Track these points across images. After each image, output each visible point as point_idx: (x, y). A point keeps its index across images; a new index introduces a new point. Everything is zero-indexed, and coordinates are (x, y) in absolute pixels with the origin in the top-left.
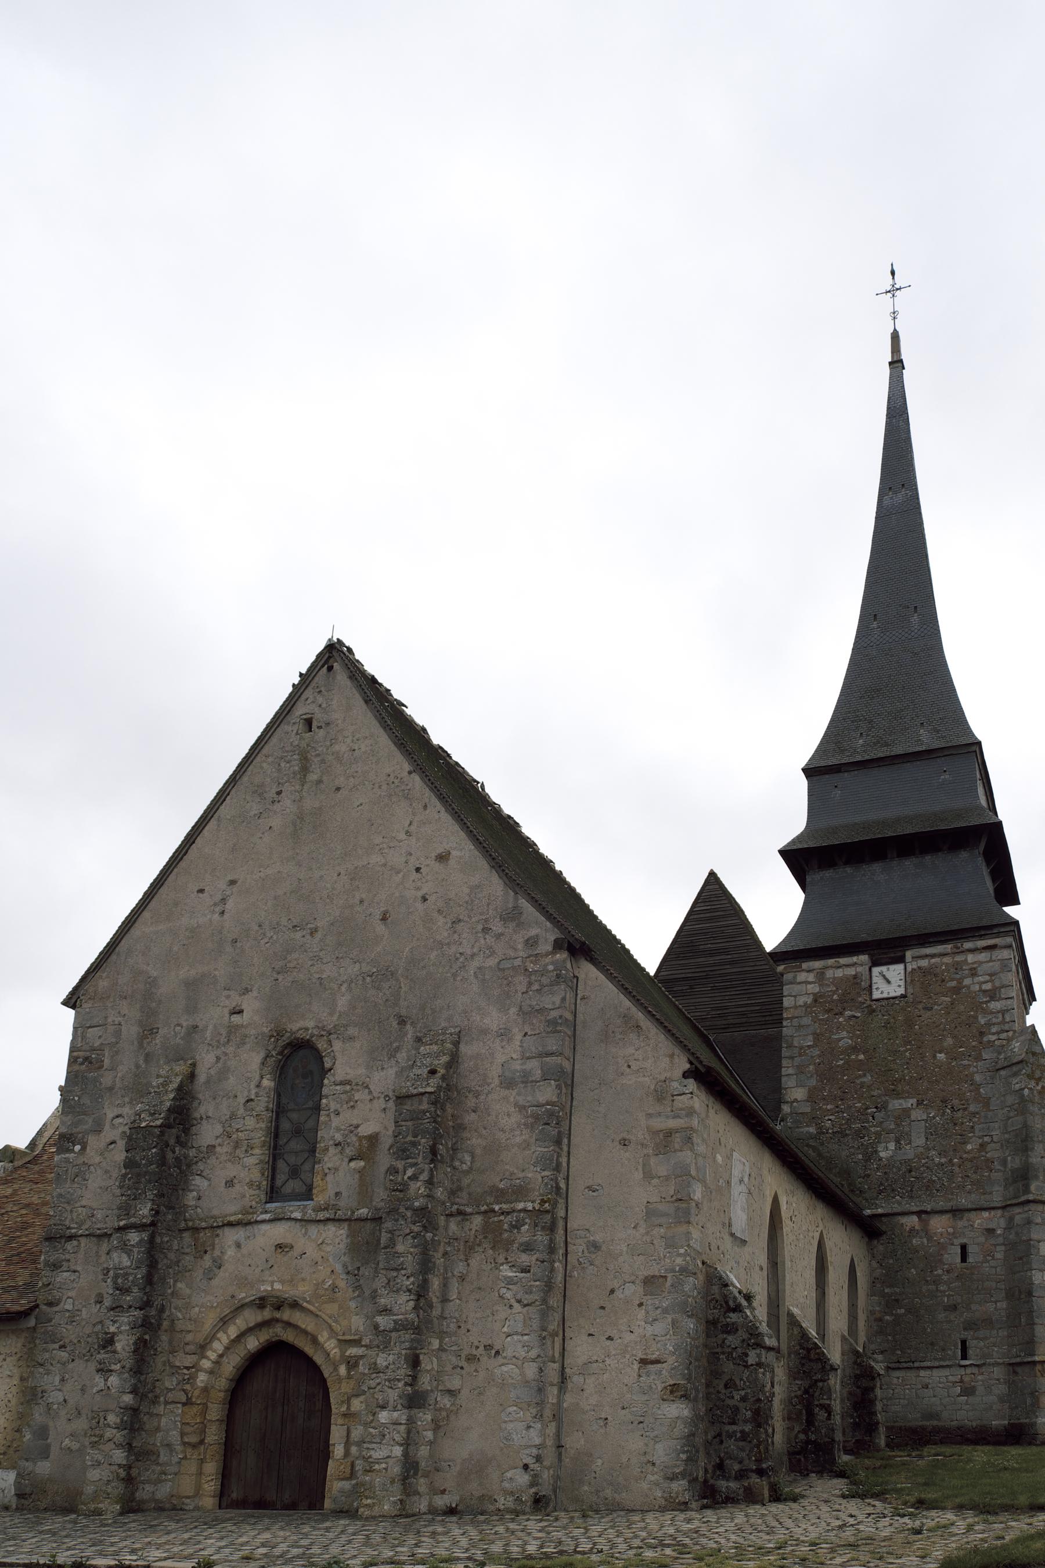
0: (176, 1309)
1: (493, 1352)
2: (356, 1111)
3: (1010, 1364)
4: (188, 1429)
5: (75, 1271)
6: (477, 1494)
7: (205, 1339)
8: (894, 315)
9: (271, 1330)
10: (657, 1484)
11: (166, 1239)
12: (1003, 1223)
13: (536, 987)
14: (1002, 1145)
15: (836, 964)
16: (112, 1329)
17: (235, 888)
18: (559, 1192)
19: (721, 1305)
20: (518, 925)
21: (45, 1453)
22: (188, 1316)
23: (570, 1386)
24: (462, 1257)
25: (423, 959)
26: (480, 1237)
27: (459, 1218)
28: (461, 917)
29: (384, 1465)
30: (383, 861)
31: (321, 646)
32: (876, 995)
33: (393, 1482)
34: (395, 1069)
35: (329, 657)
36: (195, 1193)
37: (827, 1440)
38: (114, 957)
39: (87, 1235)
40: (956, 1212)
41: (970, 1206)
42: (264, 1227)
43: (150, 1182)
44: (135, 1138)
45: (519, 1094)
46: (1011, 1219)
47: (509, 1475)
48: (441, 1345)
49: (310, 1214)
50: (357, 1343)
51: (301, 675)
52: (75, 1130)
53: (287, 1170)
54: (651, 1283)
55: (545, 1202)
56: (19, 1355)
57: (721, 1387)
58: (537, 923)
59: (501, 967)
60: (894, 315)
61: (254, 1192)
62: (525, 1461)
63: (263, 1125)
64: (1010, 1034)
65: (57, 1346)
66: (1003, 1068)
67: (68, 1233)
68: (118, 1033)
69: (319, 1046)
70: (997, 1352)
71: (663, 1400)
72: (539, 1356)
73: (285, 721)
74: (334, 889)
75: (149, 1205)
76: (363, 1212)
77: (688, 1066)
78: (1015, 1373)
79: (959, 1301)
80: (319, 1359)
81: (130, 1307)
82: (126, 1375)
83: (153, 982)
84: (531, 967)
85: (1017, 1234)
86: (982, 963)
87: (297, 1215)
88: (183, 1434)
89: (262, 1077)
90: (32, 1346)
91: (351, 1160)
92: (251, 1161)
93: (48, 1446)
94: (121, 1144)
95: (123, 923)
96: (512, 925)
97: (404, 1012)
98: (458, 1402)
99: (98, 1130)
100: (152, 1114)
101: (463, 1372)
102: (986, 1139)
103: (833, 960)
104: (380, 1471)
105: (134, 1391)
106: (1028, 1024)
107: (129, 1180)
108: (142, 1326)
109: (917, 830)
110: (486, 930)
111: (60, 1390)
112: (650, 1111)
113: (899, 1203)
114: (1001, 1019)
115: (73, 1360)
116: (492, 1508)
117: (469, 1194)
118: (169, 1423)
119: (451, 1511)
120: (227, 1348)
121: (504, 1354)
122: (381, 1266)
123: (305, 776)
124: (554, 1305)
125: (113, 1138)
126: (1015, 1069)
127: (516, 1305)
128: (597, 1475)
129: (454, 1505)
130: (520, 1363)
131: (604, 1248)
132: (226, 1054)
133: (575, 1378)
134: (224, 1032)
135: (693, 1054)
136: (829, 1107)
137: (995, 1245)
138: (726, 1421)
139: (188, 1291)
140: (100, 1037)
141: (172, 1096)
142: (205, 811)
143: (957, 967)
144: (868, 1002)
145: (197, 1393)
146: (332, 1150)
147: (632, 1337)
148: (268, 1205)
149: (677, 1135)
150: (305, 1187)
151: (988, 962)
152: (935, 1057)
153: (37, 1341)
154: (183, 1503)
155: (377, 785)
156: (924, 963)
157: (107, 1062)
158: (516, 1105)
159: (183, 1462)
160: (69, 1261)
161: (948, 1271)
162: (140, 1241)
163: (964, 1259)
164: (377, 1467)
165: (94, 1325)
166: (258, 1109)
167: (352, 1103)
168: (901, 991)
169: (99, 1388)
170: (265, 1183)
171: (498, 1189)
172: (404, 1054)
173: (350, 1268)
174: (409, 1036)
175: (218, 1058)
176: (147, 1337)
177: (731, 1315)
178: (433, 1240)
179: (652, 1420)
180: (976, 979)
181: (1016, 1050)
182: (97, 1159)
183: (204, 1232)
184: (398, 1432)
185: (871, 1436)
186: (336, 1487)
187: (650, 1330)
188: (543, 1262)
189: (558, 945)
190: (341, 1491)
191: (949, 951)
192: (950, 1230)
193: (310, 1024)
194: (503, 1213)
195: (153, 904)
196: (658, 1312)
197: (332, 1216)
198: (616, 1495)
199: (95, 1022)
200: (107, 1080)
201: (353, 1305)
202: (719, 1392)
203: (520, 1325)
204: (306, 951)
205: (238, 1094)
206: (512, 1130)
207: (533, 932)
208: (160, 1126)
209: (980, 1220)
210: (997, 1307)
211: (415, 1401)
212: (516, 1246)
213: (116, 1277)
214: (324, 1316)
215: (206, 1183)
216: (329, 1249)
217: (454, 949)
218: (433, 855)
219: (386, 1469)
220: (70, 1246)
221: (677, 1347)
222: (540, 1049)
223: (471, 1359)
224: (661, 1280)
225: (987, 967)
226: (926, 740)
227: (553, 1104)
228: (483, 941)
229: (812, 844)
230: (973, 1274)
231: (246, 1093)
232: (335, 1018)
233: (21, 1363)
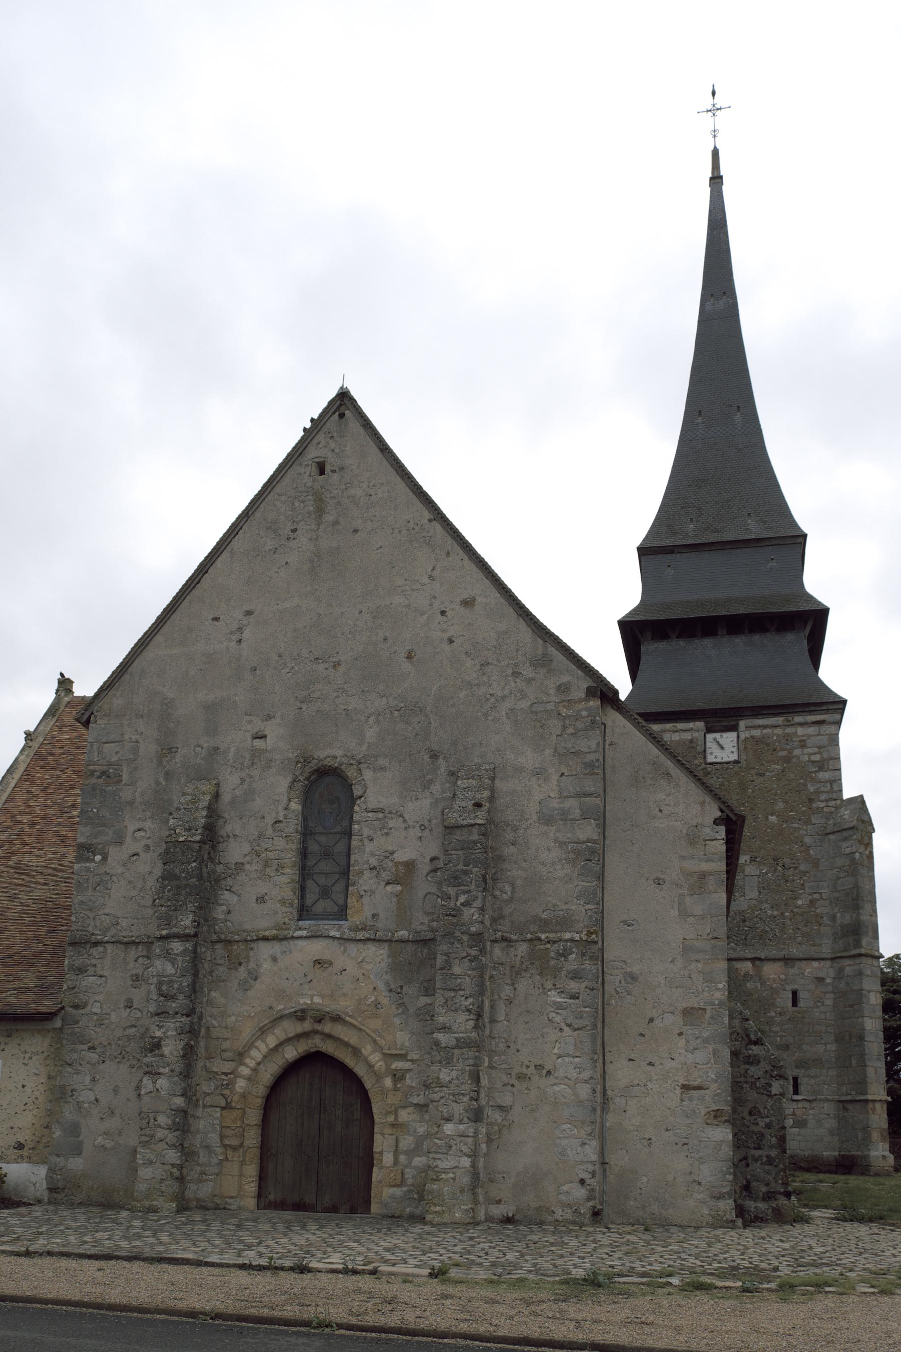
0: (210, 1017)
1: (544, 1072)
3: (840, 1101)
4: (228, 1132)
5: (101, 976)
7: (244, 1047)
8: (715, 134)
9: (309, 1041)
10: (703, 1202)
11: (203, 950)
12: (832, 973)
13: (571, 730)
14: (831, 903)
15: (674, 729)
16: (158, 1034)
18: (599, 923)
19: (742, 1038)
21: (77, 1150)
23: (612, 1106)
24: (509, 981)
25: (452, 698)
26: (527, 963)
27: (504, 944)
29: (451, 1175)
30: (407, 602)
31: (332, 394)
32: (710, 759)
33: (462, 1191)
34: (429, 800)
35: (341, 405)
36: (224, 908)
38: (126, 677)
39: (113, 942)
40: (788, 961)
41: (801, 956)
42: (300, 943)
43: (190, 894)
45: (558, 830)
46: (841, 970)
47: (565, 1188)
48: (490, 1063)
49: (348, 934)
50: (402, 1057)
51: (312, 420)
52: (94, 841)
55: (592, 933)
56: (46, 1054)
57: (746, 1114)
58: (567, 671)
59: (534, 710)
60: (715, 134)
61: (287, 910)
62: (581, 1176)
63: (294, 847)
65: (86, 1047)
66: (833, 833)
68: (135, 750)
69: (349, 774)
71: (707, 1124)
72: (591, 1078)
73: (297, 462)
75: (191, 917)
76: (403, 934)
77: (719, 814)
78: (846, 1109)
80: (360, 1070)
81: (177, 1013)
82: (176, 1079)
84: (564, 712)
85: (847, 984)
88: (222, 1137)
89: (290, 800)
90: (59, 1046)
91: (388, 883)
92: (284, 879)
93: (80, 1143)
95: (136, 645)
96: (542, 671)
97: (435, 747)
98: (510, 1117)
99: (119, 841)
101: (514, 1089)
102: (816, 896)
103: (671, 725)
104: (447, 1180)
106: (846, 795)
107: (169, 891)
108: (190, 1032)
109: (750, 611)
110: (516, 674)
111: (90, 1090)
112: (683, 854)
113: (734, 950)
114: (829, 788)
115: (104, 1062)
116: (550, 1218)
117: (512, 922)
118: (207, 1125)
119: (509, 1220)
120: (265, 1057)
121: (556, 1075)
123: (320, 516)
124: (599, 1033)
125: (136, 851)
126: (845, 834)
127: (566, 1029)
129: (510, 1215)
130: (572, 1083)
132: (251, 777)
133: (617, 1100)
134: (248, 756)
135: (724, 802)
137: (825, 993)
138: (752, 1145)
139: (223, 1000)
140: (117, 753)
141: (204, 813)
142: (218, 543)
145: (236, 1098)
146: (367, 874)
147: (674, 1063)
148: (301, 923)
149: (711, 877)
150: (336, 908)
151: (817, 735)
152: (767, 818)
153: (64, 1042)
154: (226, 1203)
155: (396, 531)
156: (757, 733)
157: (125, 777)
158: (556, 840)
159: (225, 1163)
160: (95, 966)
161: (780, 1014)
163: (795, 1003)
164: (443, 1176)
165: (125, 1029)
166: (287, 830)
167: (386, 831)
168: (734, 757)
169: (148, 1090)
170: (296, 901)
171: (541, 920)
172: (438, 787)
173: (392, 986)
174: (442, 769)
175: (243, 780)
176: (192, 1043)
177: (753, 1047)
181: (846, 817)
182: (120, 870)
183: (238, 946)
184: (466, 1144)
186: (385, 1192)
187: (690, 1058)
188: (592, 990)
190: (393, 1197)
191: (781, 723)
192: (783, 977)
193: (339, 753)
194: (549, 942)
195: (166, 629)
196: (699, 1041)
197: (373, 937)
198: (662, 1211)
200: (126, 794)
201: (397, 1021)
202: (743, 1118)
204: (330, 683)
206: (553, 864)
207: (565, 679)
208: (199, 842)
209: (811, 969)
210: (827, 1049)
212: (564, 973)
213: (160, 984)
214: (367, 1030)
215: (236, 898)
216: (369, 967)
218: (458, 600)
219: (454, 1179)
220: (96, 951)
223: (521, 1077)
224: (701, 1012)
226: (753, 529)
227: (594, 842)
228: (513, 684)
229: (638, 618)
230: (804, 1017)
231: (274, 815)
232: (364, 748)
233: (48, 1062)
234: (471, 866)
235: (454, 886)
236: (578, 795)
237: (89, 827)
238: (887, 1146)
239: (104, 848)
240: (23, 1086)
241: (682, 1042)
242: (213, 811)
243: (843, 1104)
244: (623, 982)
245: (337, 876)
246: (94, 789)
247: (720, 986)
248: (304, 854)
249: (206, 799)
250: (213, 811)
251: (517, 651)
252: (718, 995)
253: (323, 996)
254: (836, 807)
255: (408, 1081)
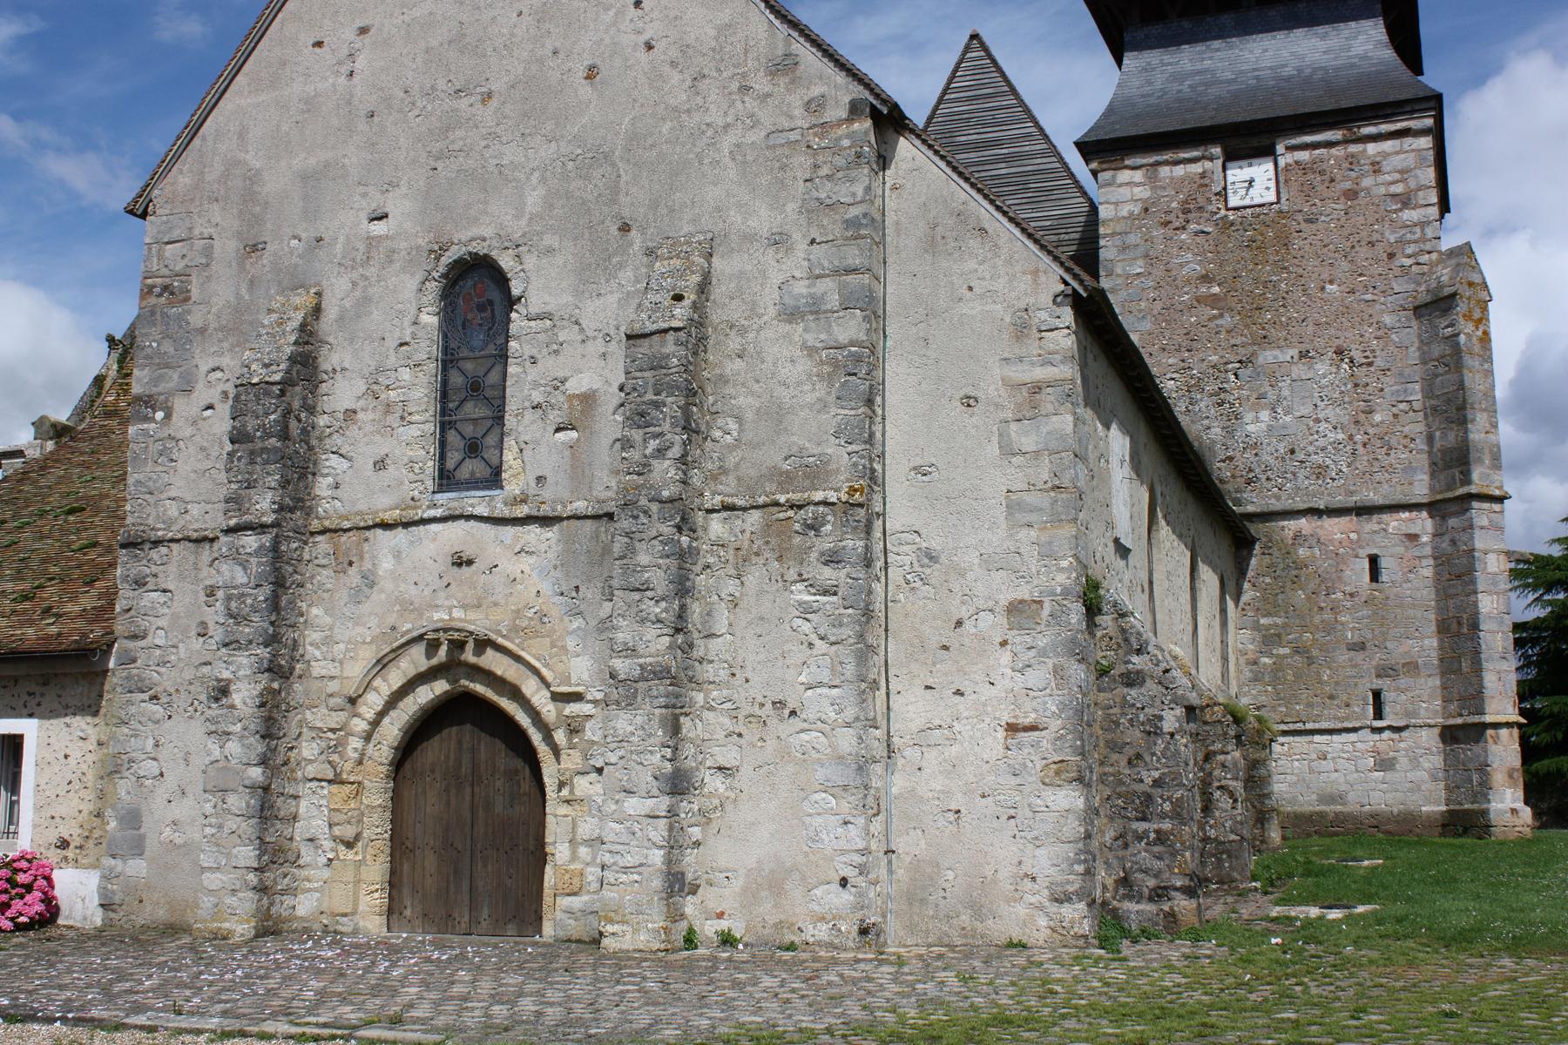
1: (787, 712)
2: (561, 358)
5: (164, 591)
6: (772, 919)
10: (1041, 908)
13: (825, 171)
16: (226, 675)
17: (367, 39)
20: (793, 81)
22: (330, 656)
23: (900, 762)
24: (733, 572)
25: (652, 134)
27: (725, 514)
28: (706, 71)
34: (617, 296)
36: (330, 479)
37: (1233, 837)
41: (1381, 502)
43: (267, 462)
44: (245, 395)
49: (502, 510)
52: (155, 390)
53: (462, 443)
54: (1015, 609)
57: (1123, 763)
58: (821, 78)
62: (842, 874)
64: (1434, 256)
67: (153, 536)
68: (208, 252)
70: (1427, 709)
74: (512, 35)
75: (269, 495)
79: (1369, 636)
81: (250, 642)
83: (253, 177)
84: (815, 142)
85: (1453, 542)
86: (1389, 155)
87: (481, 510)
91: (558, 430)
92: (414, 431)
93: (142, 838)
94: (224, 409)
96: (783, 81)
97: (626, 213)
100: (266, 366)
101: (742, 741)
105: (264, 762)
112: (1006, 355)
117: (739, 479)
118: (313, 812)
122: (615, 583)
127: (818, 643)
128: (948, 894)
131: (943, 559)
133: (908, 752)
134: (362, 247)
136: (1171, 361)
139: (328, 620)
143: (1352, 160)
144: (1223, 212)
145: (348, 766)
146: (529, 415)
147: (993, 691)
148: (438, 496)
150: (489, 471)
152: (1323, 289)
157: (195, 293)
158: (804, 347)
160: (155, 576)
161: (1351, 595)
162: (260, 547)
163: (1375, 574)
173: (564, 588)
175: (354, 284)
178: (690, 547)
179: (1029, 814)
180: (1381, 178)
182: (188, 432)
185: (1263, 828)
189: (855, 109)
193: (488, 232)
194: (791, 507)
196: (1033, 653)
199: (175, 234)
200: (196, 319)
203: (827, 672)
205: (387, 335)
206: (799, 384)
207: (816, 91)
209: (1396, 523)
210: (1428, 645)
211: (678, 784)
212: (814, 555)
213: (229, 598)
215: (345, 464)
217: (697, 117)
221: (1063, 707)
222: (836, 263)
224: (1034, 606)
225: (1397, 161)
231: (397, 334)
232: (523, 222)
234: (664, 394)
235: (639, 427)
236: (836, 272)
237: (146, 371)
238: (1520, 794)
239: (167, 400)
240: (66, 757)
241: (1005, 657)
242: (308, 334)
243: (1450, 735)
244: (916, 564)
245: (489, 423)
246: (153, 313)
247: (1065, 564)
248: (444, 394)
249: (298, 317)
250: (308, 334)
251: (746, 52)
252: (1061, 578)
253: (465, 607)
254: (1431, 264)
255: (588, 735)
